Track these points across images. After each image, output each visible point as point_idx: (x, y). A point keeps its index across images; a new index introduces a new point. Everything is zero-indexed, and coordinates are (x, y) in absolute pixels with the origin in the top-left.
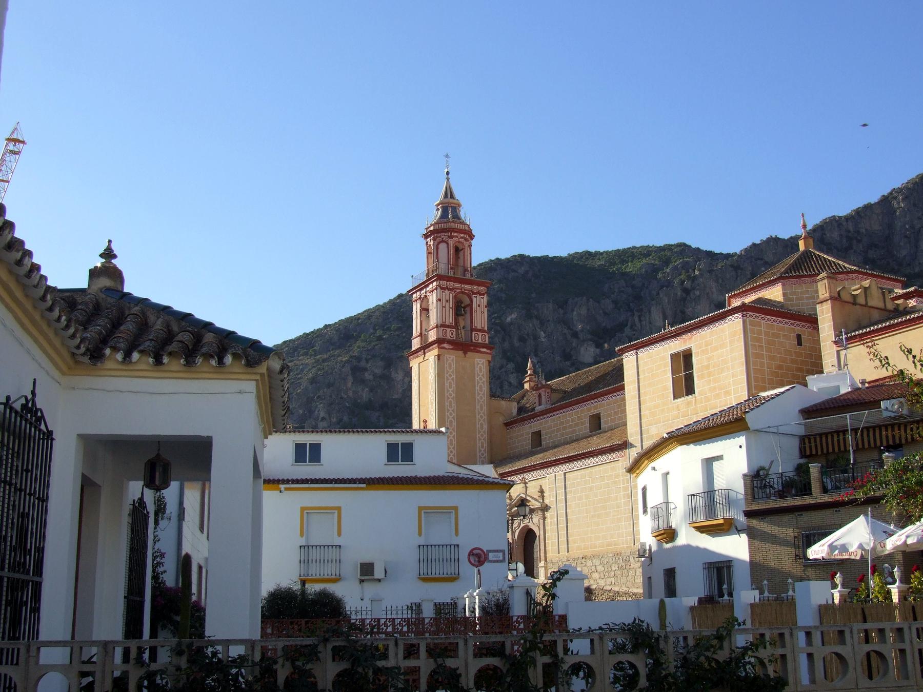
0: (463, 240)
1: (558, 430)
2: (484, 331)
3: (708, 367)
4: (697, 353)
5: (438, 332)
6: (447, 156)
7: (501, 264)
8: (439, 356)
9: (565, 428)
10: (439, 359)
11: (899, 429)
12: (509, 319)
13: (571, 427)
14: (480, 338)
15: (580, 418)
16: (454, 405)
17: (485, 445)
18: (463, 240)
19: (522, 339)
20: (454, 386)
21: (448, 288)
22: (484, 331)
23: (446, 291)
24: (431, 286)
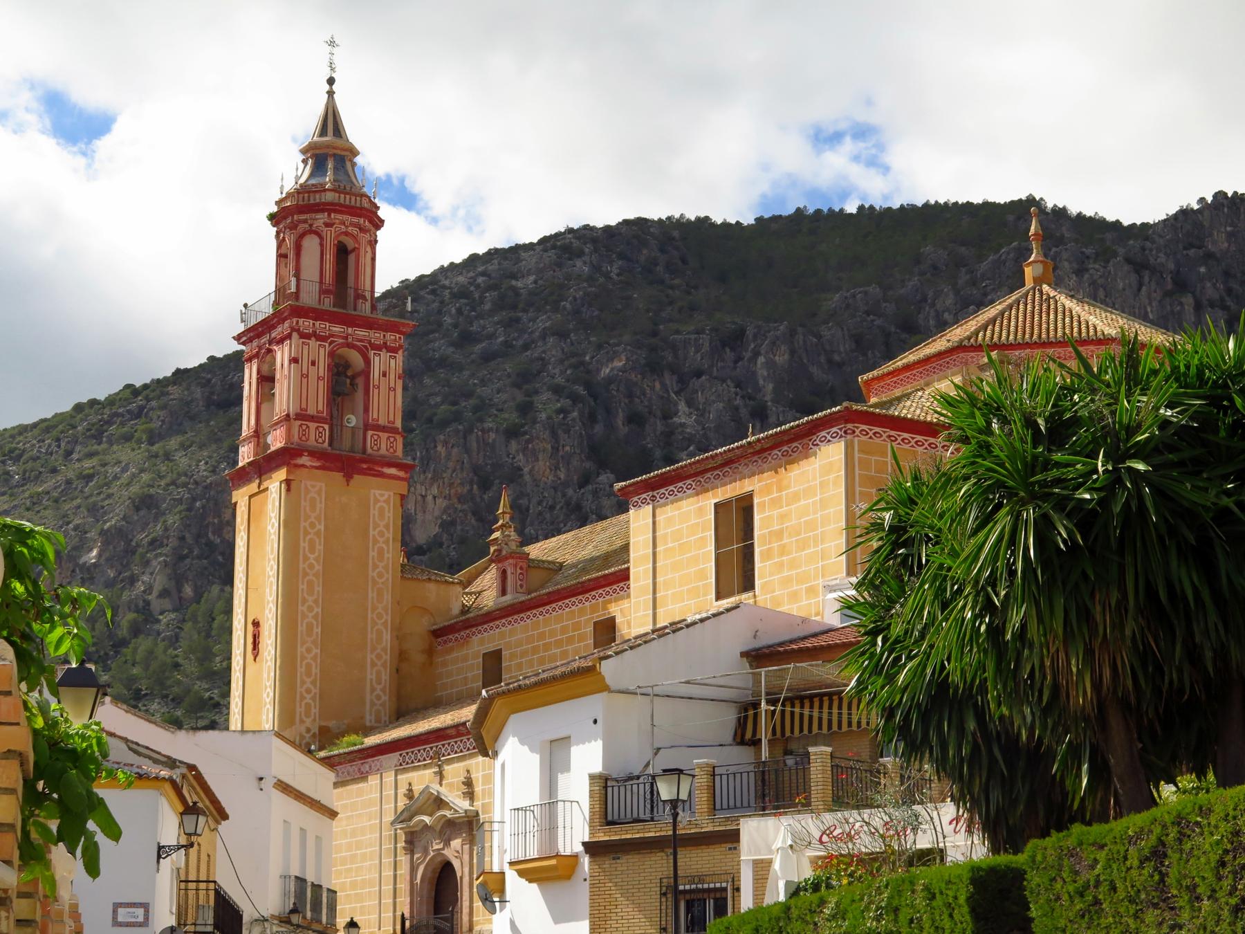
0: (354, 231)
1: (535, 650)
2: (393, 430)
3: (779, 534)
4: (762, 505)
5: (289, 431)
6: (332, 43)
7: (594, 241)
8: (288, 482)
9: (547, 647)
10: (288, 490)
11: (812, 707)
12: (605, 371)
13: (559, 643)
14: (382, 445)
15: (577, 626)
16: (318, 589)
17: (385, 677)
18: (354, 231)
19: (635, 419)
20: (319, 547)
21: (315, 335)
22: (393, 430)
23: (313, 343)
24: (279, 329)
